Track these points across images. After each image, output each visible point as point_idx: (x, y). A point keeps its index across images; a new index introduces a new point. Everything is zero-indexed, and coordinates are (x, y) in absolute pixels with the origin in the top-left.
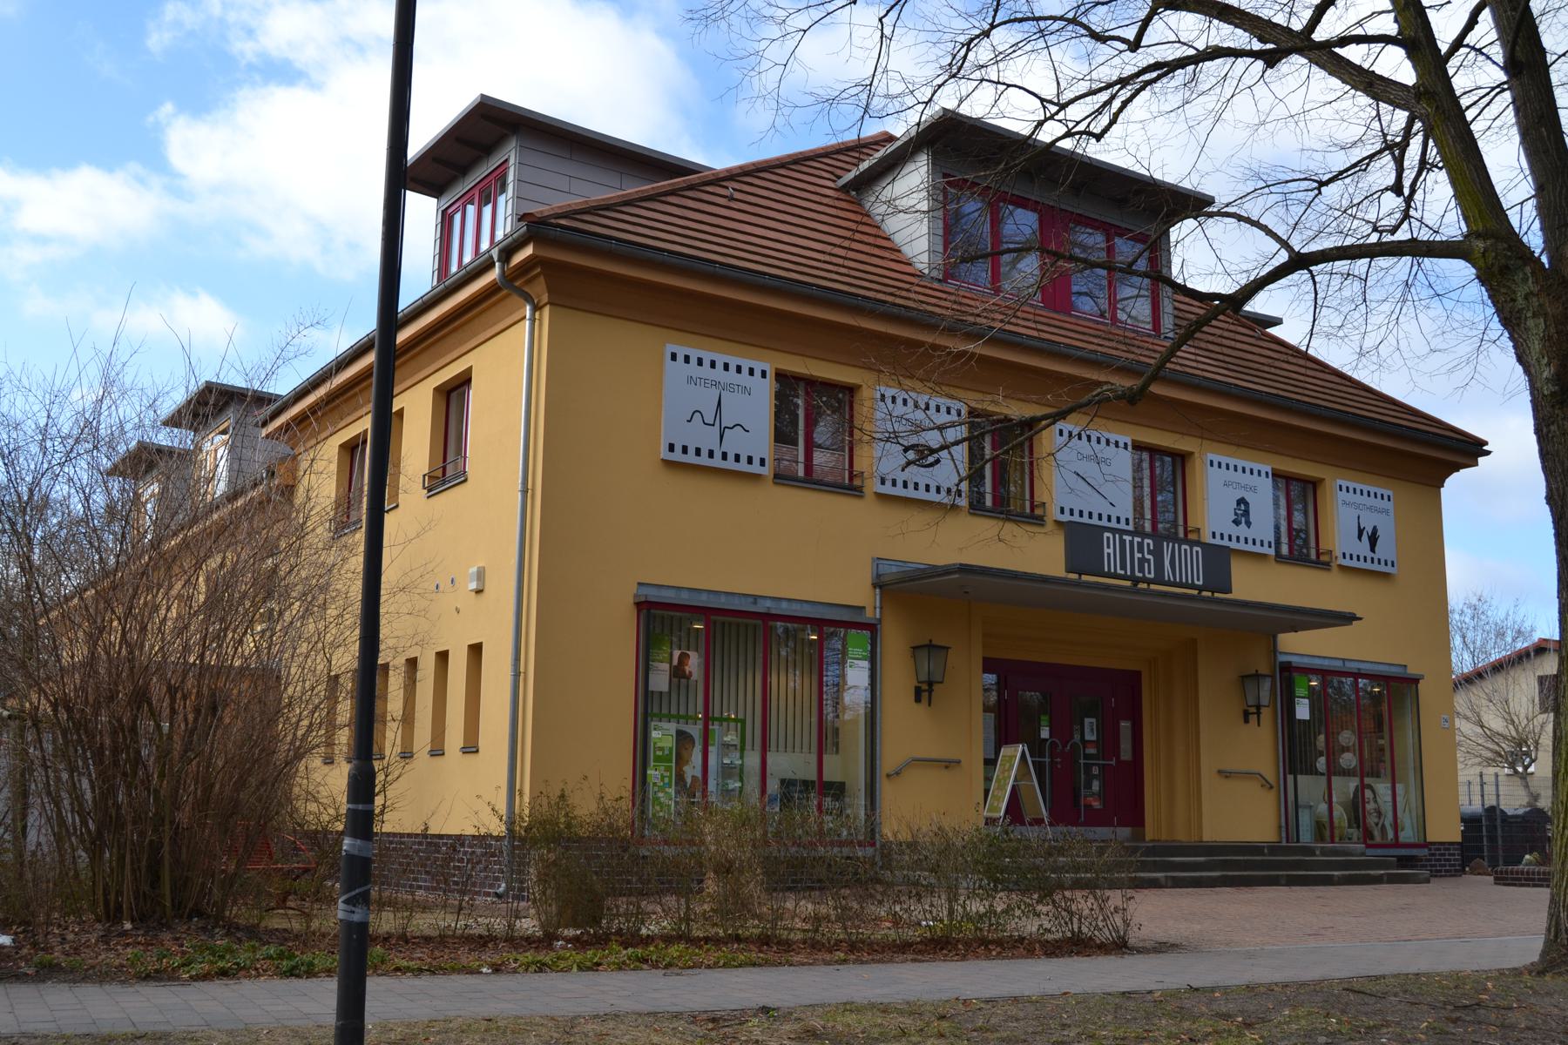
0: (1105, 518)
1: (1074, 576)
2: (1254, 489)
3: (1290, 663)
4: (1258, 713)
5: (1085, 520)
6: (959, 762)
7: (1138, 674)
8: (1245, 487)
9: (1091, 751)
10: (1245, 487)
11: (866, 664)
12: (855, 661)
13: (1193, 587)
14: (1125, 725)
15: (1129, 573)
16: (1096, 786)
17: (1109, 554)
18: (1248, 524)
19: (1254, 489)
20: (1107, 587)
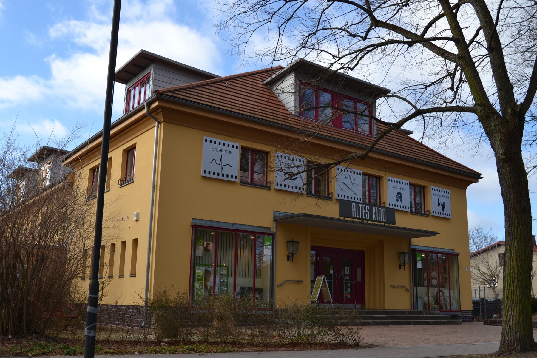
0: (353, 198)
1: (342, 218)
2: (403, 189)
3: (415, 248)
4: (404, 266)
5: (346, 199)
8: (400, 188)
9: (347, 278)
11: (271, 247)
12: (267, 246)
13: (382, 222)
14: (359, 269)
15: (361, 217)
16: (349, 290)
18: (401, 201)
19: (403, 189)
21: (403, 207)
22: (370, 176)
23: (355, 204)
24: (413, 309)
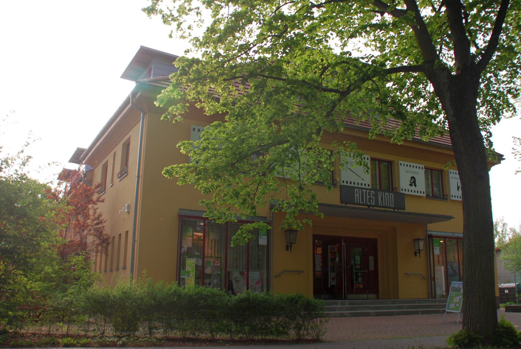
0: (360, 184)
1: (344, 205)
2: (417, 173)
3: (431, 234)
4: (419, 253)
5: (349, 184)
6: (303, 272)
7: (376, 240)
8: (414, 173)
9: (358, 267)
10: (414, 173)
11: (266, 237)
12: (262, 236)
13: (390, 208)
14: (371, 258)
15: (365, 203)
16: (360, 280)
17: (357, 196)
18: (415, 185)
19: (417, 173)
20: (354, 208)
21: (421, 192)
22: (380, 161)
23: (357, 190)
24: (430, 297)
